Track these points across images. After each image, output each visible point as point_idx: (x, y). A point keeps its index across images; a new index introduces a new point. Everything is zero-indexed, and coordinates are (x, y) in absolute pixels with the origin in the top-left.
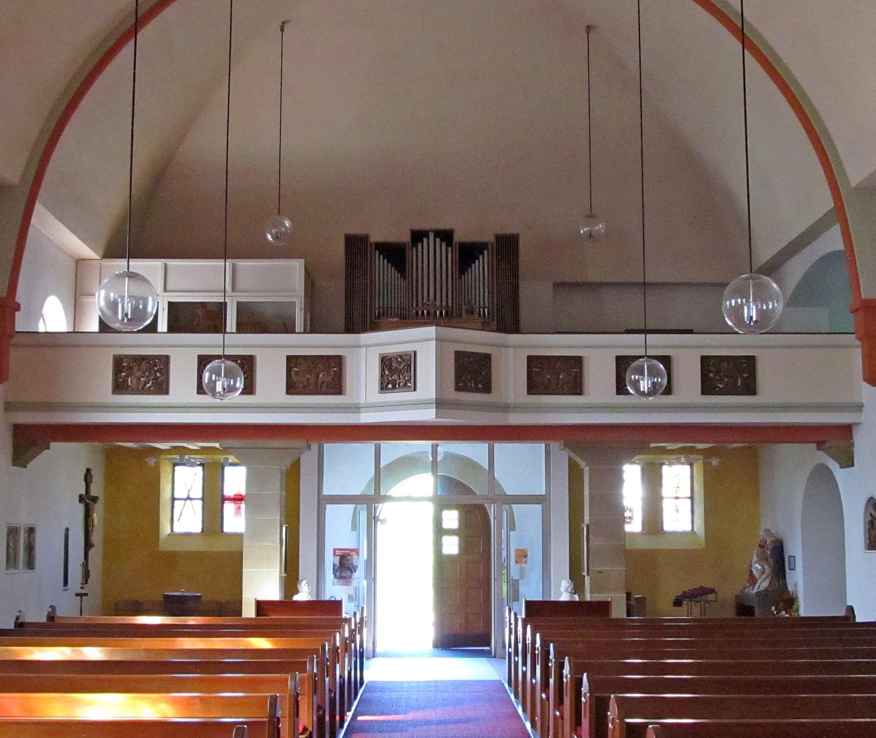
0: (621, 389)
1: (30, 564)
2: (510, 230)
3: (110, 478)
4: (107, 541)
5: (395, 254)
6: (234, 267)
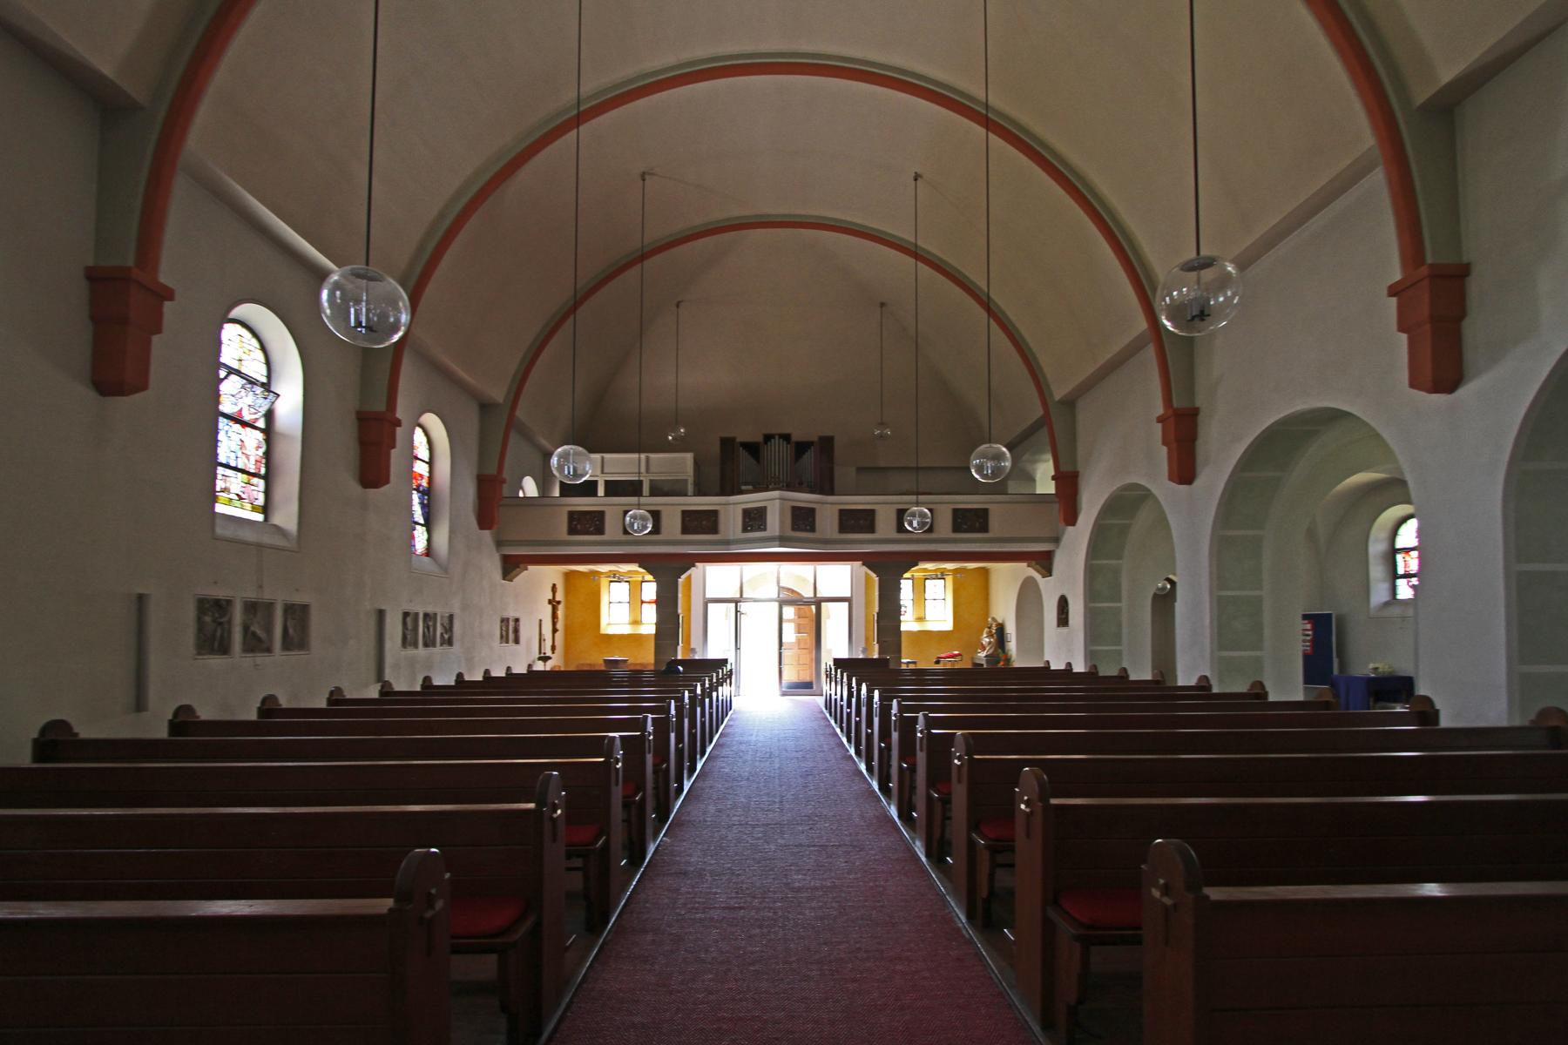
0: (901, 528)
1: (517, 641)
2: (828, 433)
3: (567, 592)
4: (567, 628)
5: (753, 449)
6: (648, 459)
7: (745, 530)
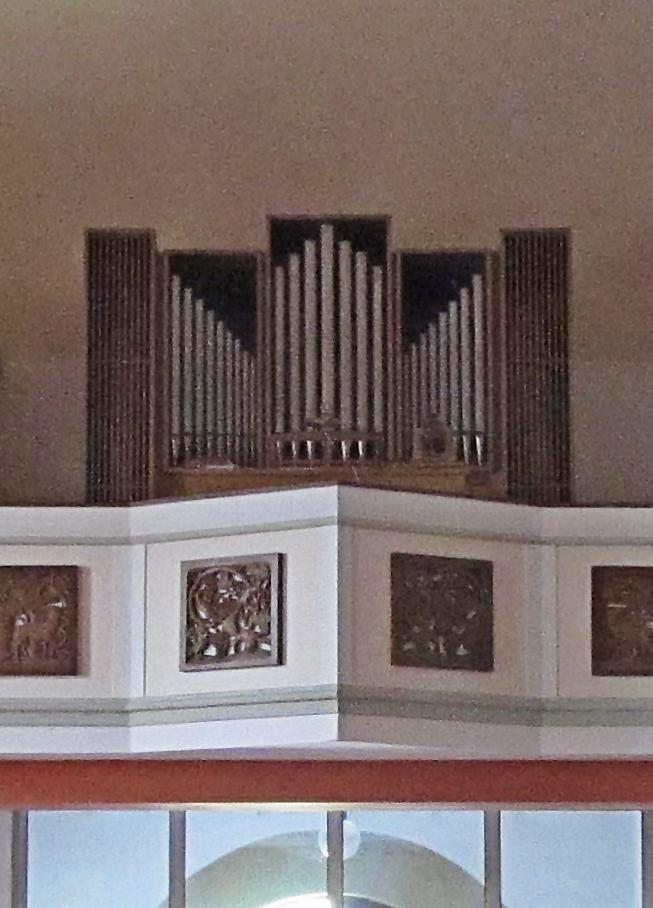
5: (227, 286)
7: (193, 657)
